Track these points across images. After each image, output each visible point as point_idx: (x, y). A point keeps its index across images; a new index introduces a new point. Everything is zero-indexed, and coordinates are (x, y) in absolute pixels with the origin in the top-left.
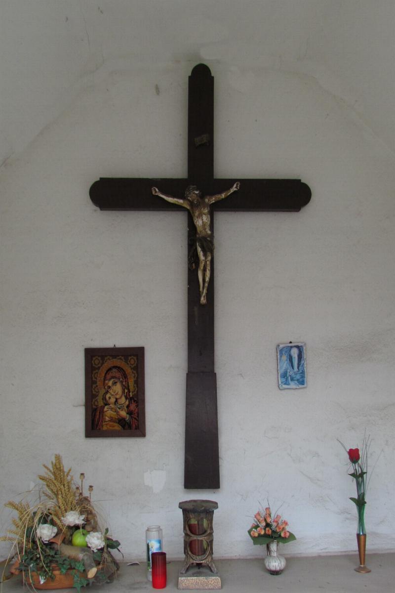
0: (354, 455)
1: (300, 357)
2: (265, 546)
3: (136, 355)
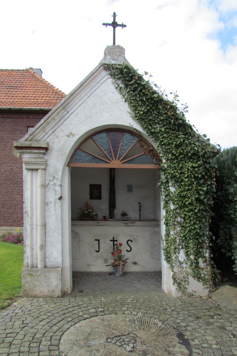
0: (139, 203)
1: (131, 187)
2: (116, 44)
3: (100, 186)
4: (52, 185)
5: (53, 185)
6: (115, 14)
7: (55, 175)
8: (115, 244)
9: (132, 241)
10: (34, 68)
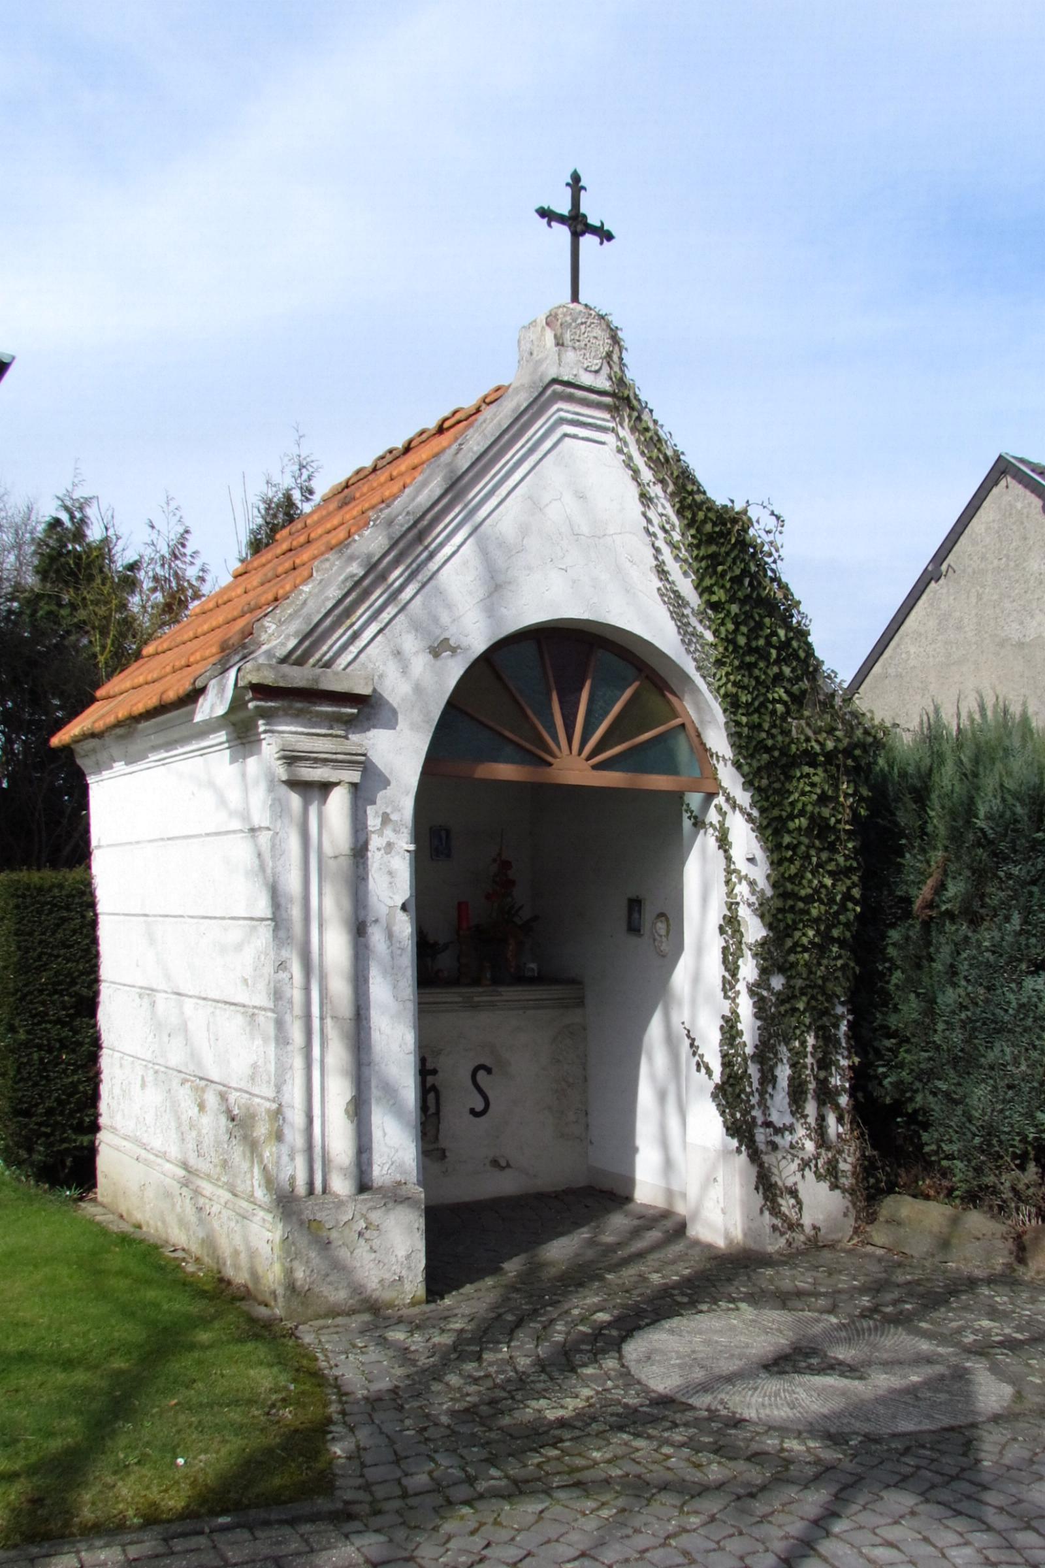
4: (379, 849)
5: (382, 851)
6: (576, 178)
7: (388, 811)
8: (428, 1085)
9: (489, 1071)
10: (468, 402)
